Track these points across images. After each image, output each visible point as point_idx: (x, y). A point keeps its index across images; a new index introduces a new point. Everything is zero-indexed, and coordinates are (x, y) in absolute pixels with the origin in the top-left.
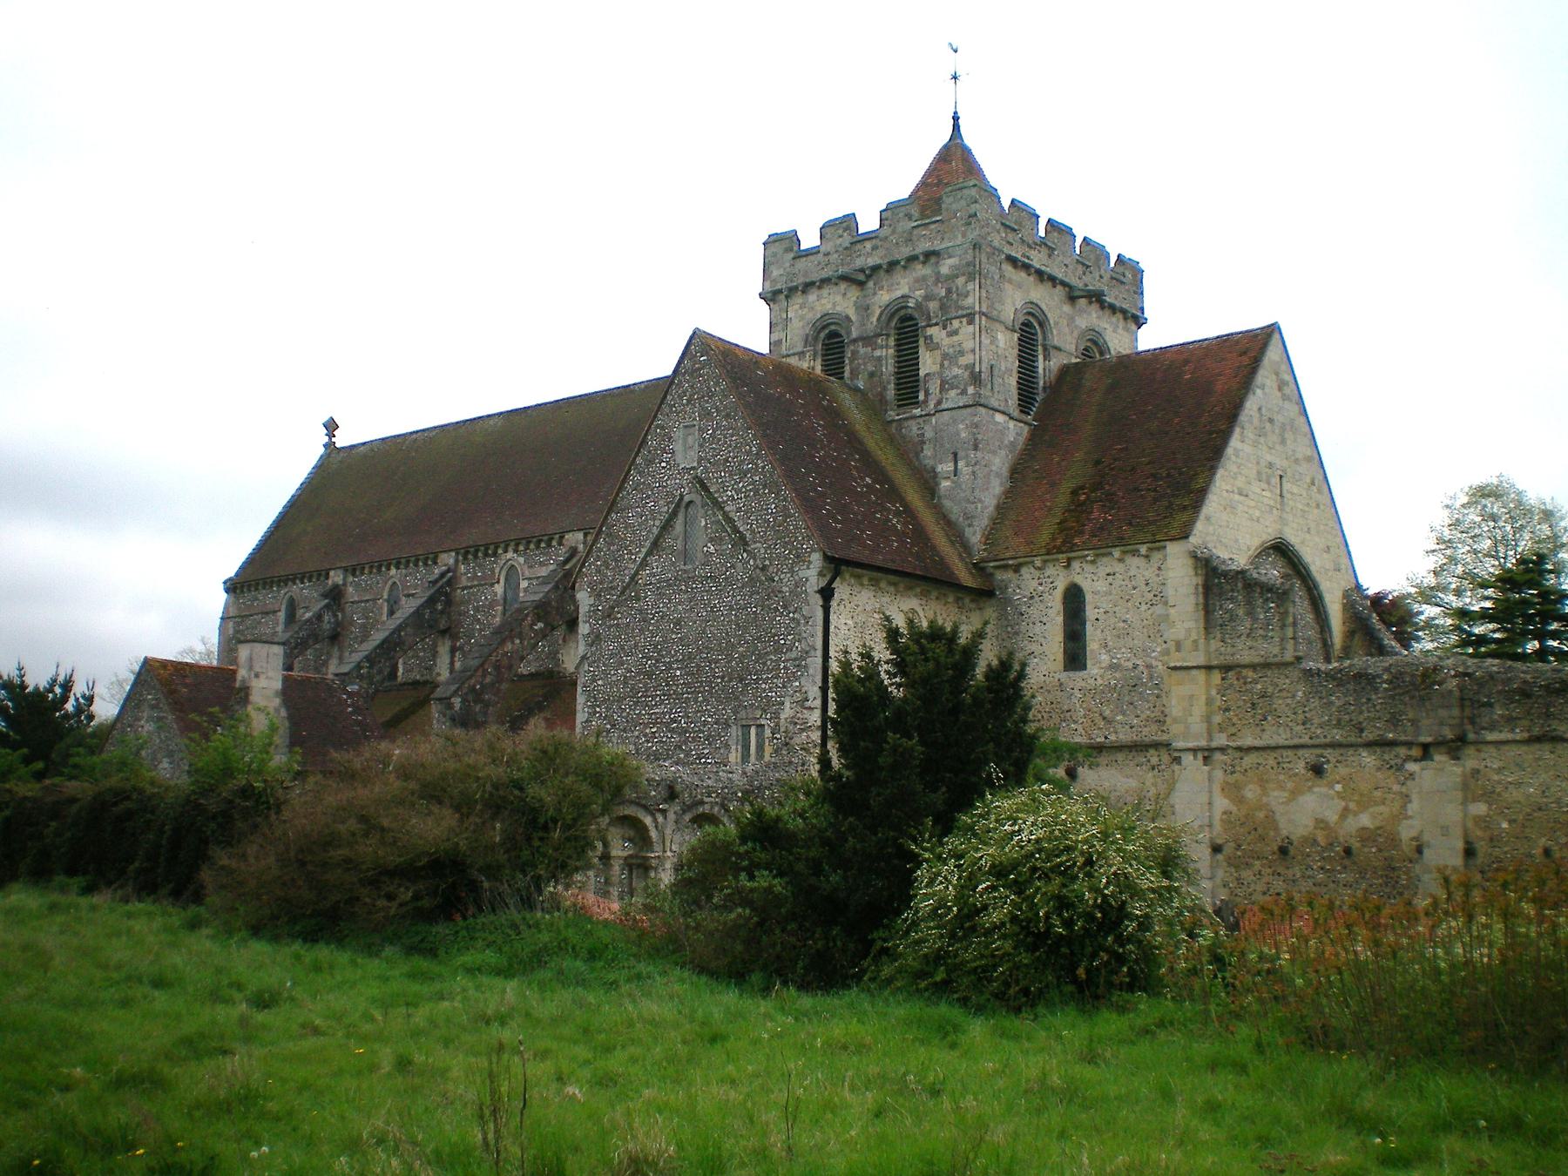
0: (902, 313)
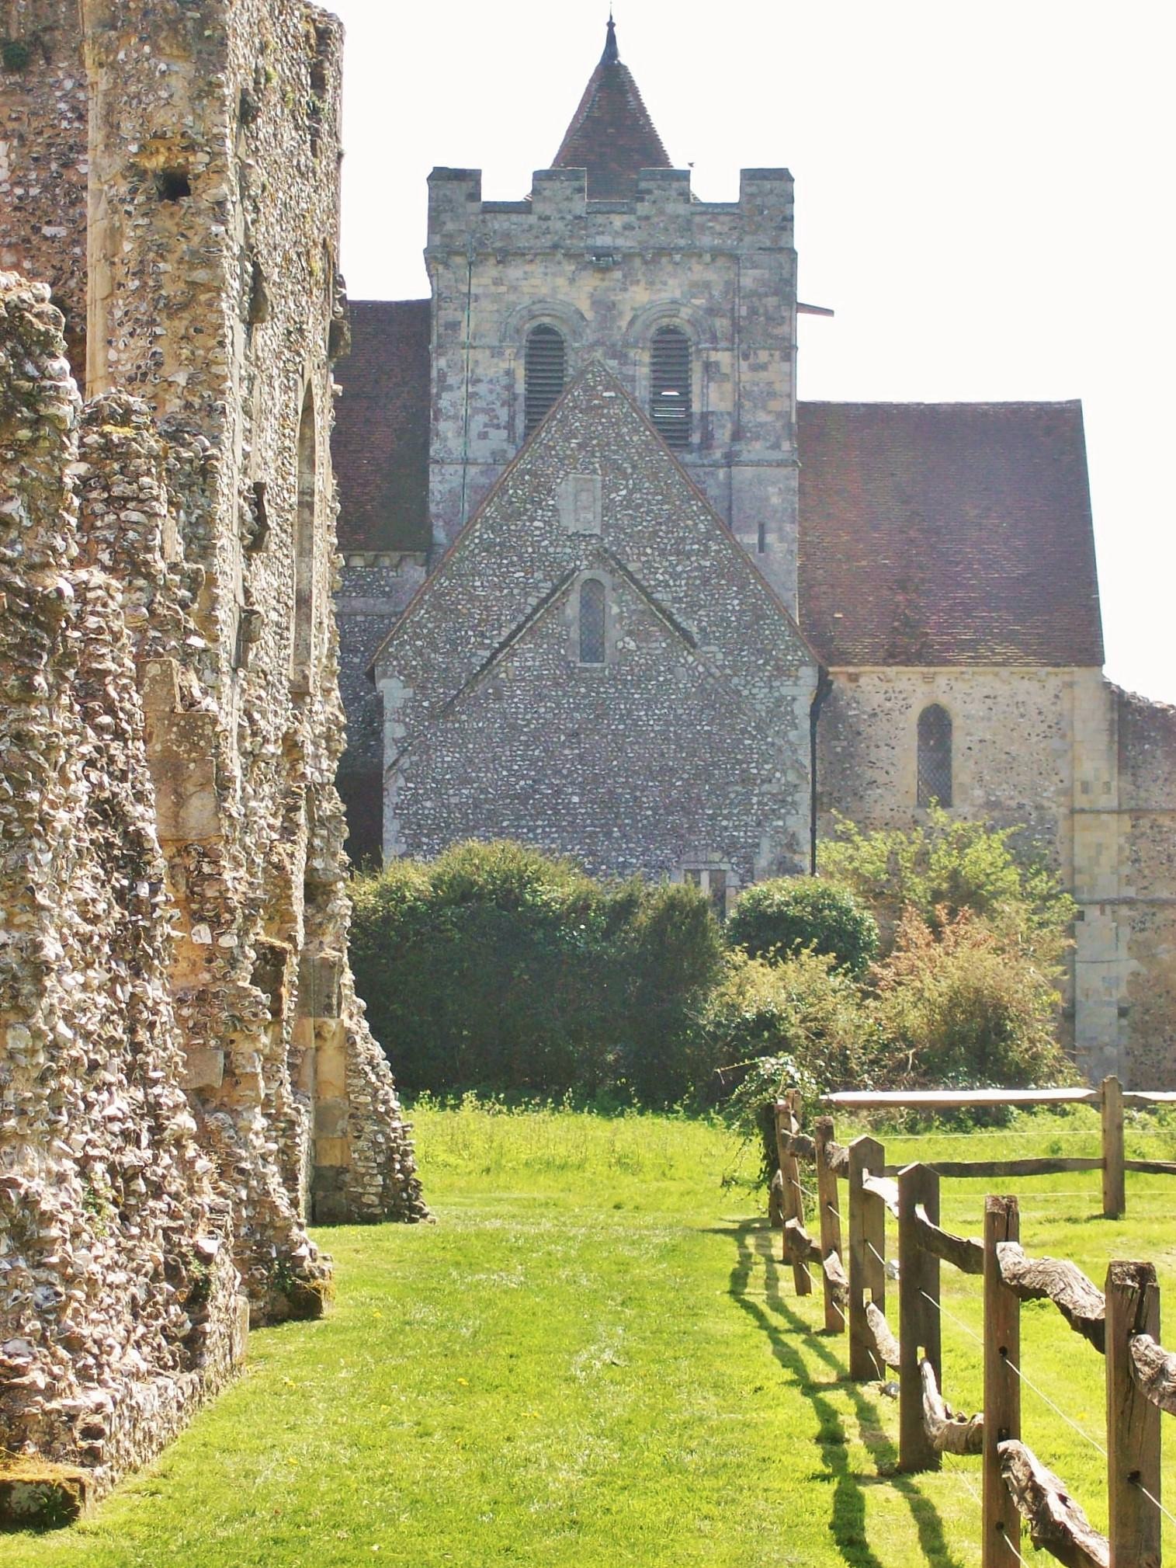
0: (665, 321)
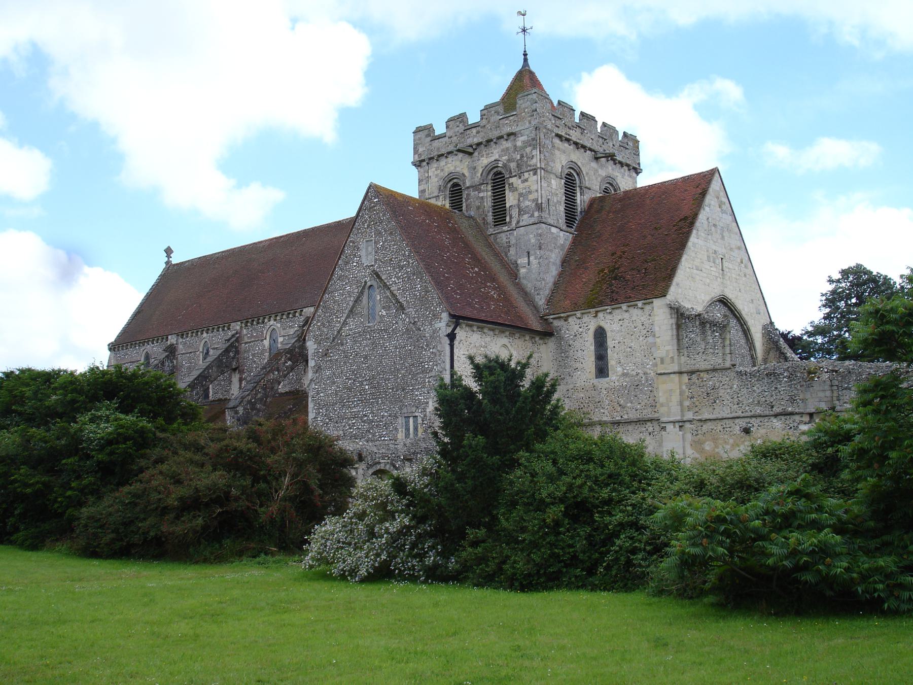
0: (495, 170)
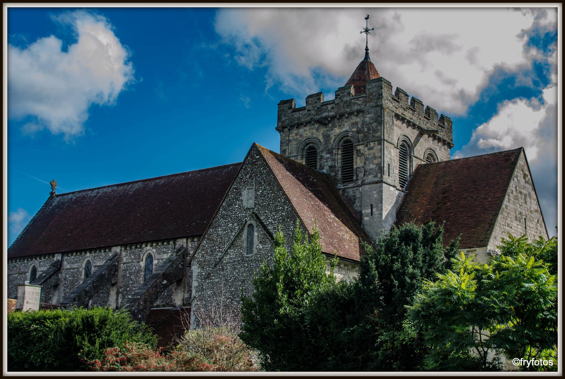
0: (346, 138)
